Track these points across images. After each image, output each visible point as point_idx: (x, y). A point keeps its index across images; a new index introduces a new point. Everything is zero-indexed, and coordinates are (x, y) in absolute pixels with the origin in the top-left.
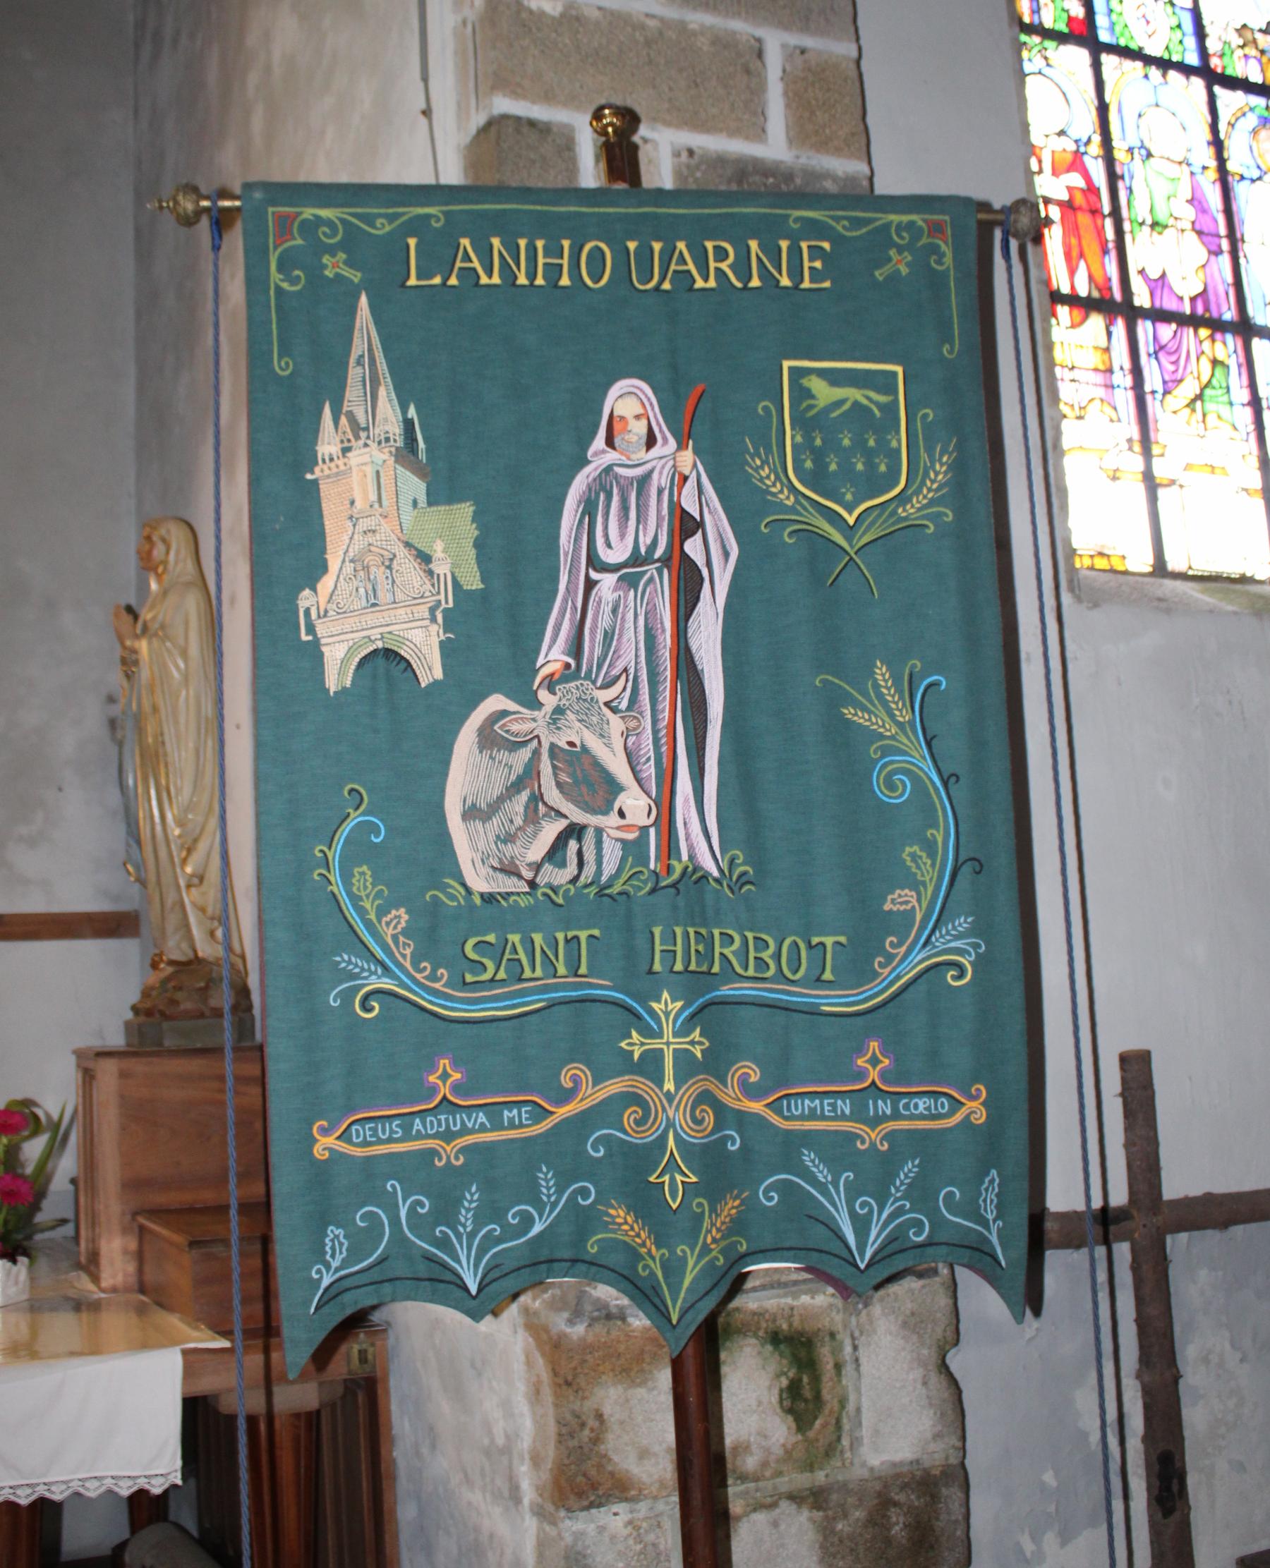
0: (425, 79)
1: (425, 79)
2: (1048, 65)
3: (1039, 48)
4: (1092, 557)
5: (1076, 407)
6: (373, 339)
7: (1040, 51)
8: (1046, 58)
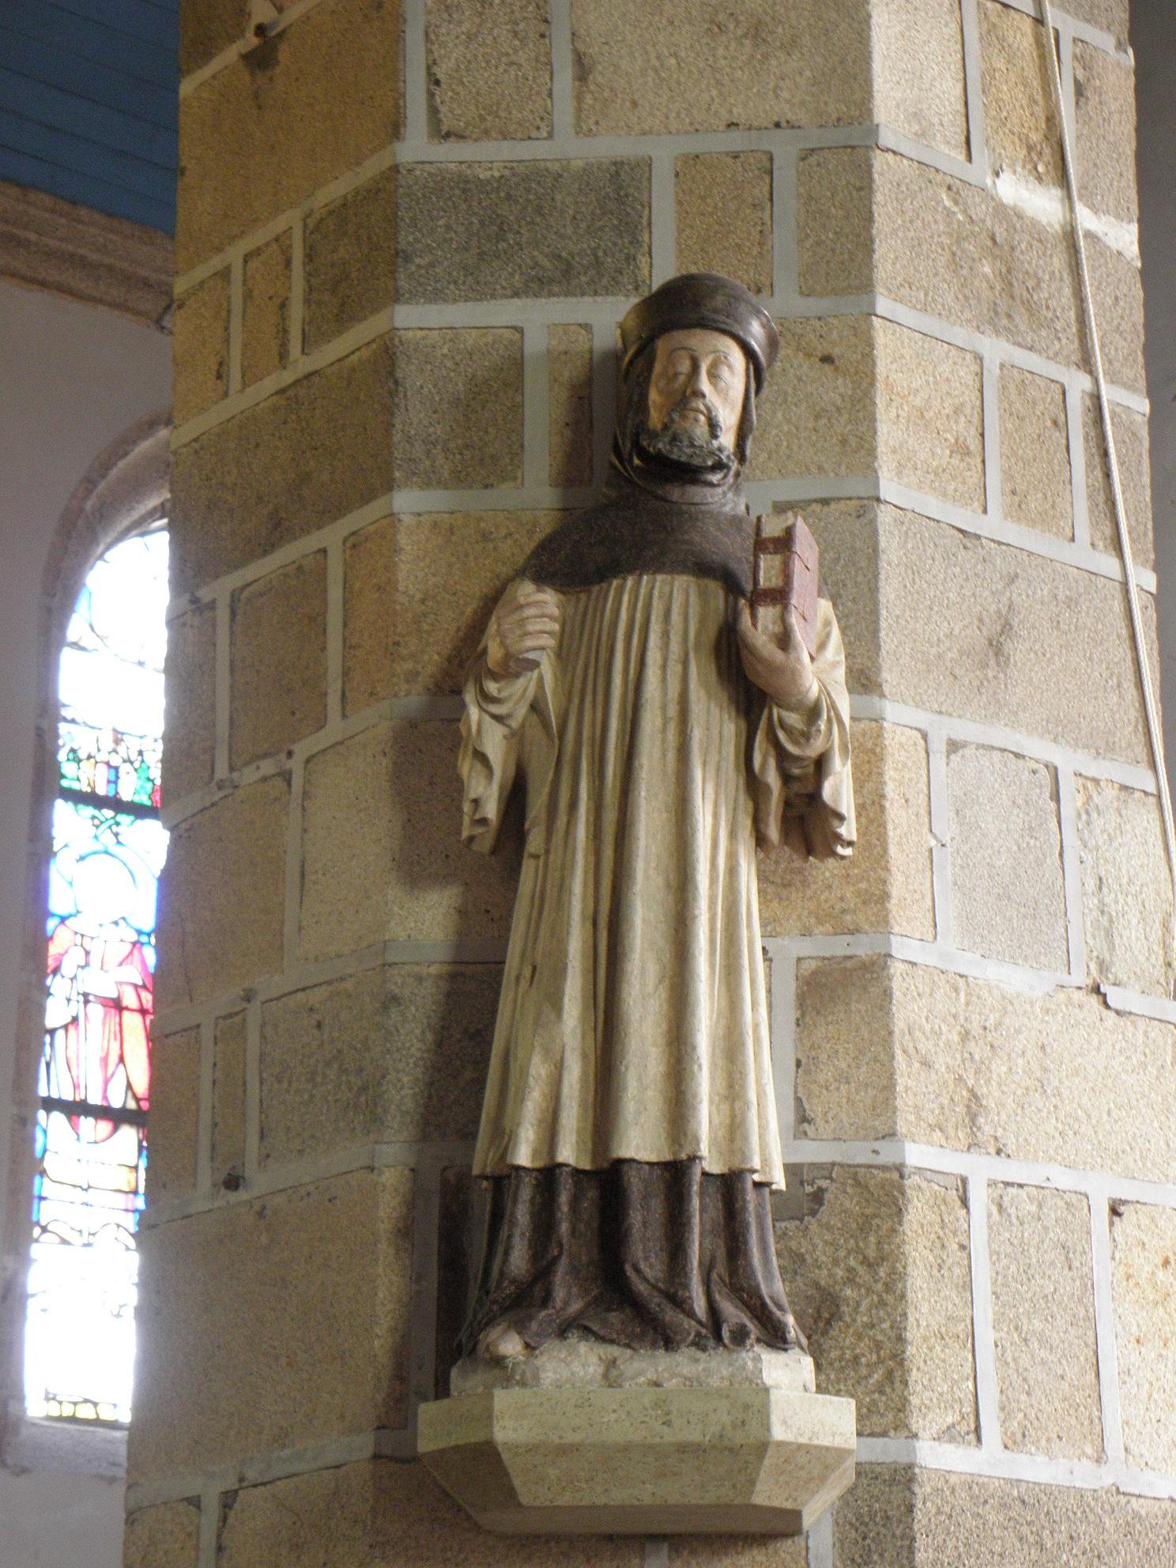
0: (960, 9)
1: (960, 9)
2: (118, 842)
3: (112, 822)
4: (75, 1404)
5: (85, 1233)
6: (656, 1231)
7: (110, 827)
8: (116, 835)
